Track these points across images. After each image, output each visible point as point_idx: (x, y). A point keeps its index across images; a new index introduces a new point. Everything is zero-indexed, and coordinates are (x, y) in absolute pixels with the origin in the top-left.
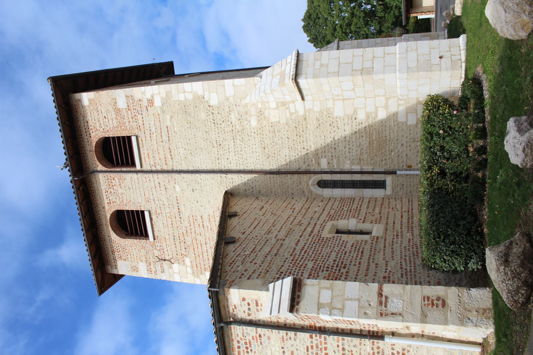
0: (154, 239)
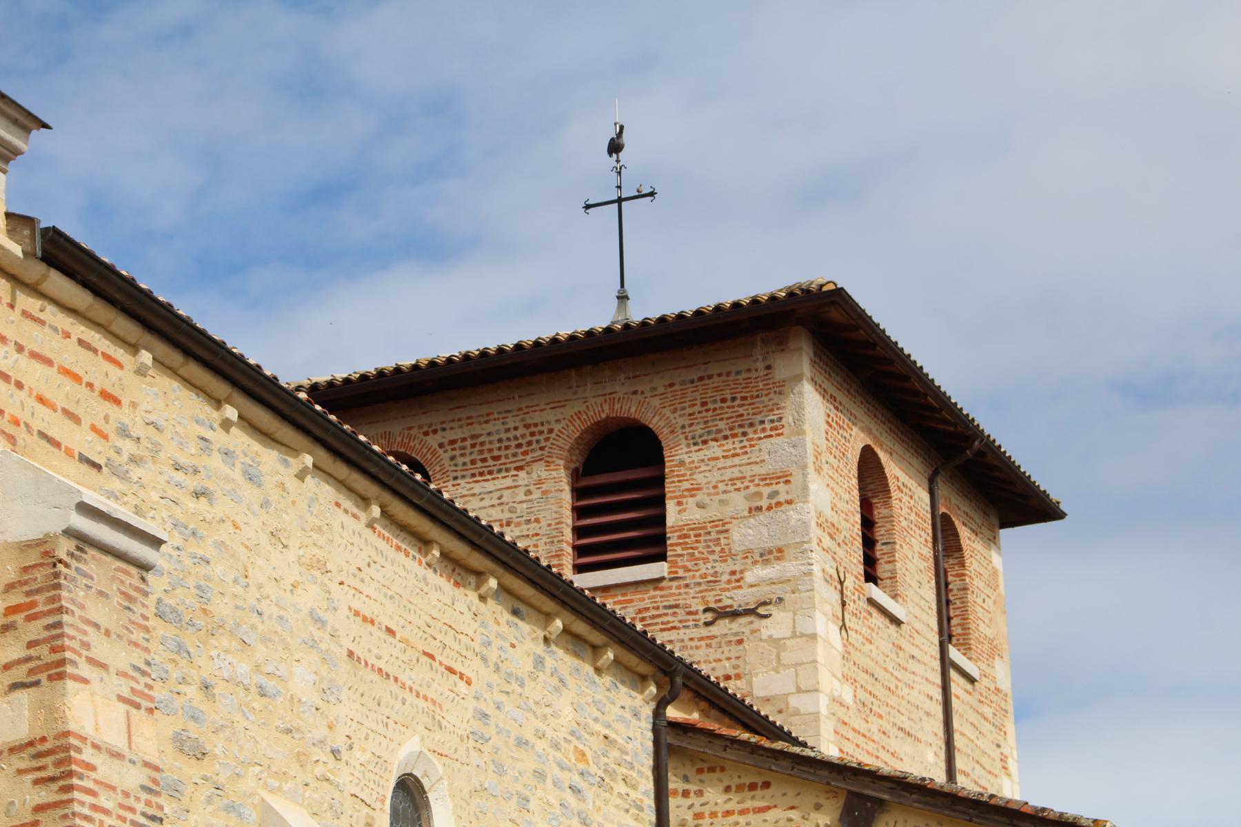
0: (871, 601)
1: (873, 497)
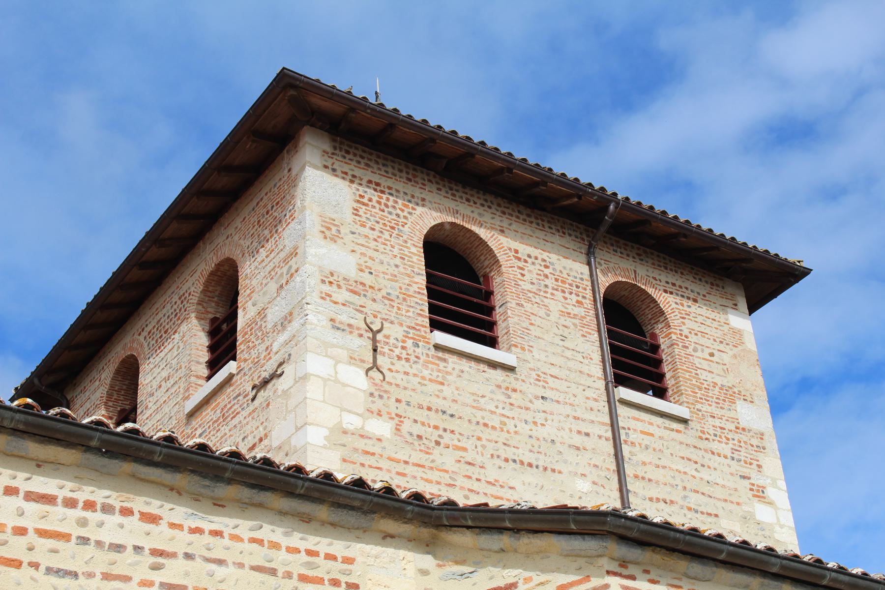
0: (437, 347)
1: (490, 272)
